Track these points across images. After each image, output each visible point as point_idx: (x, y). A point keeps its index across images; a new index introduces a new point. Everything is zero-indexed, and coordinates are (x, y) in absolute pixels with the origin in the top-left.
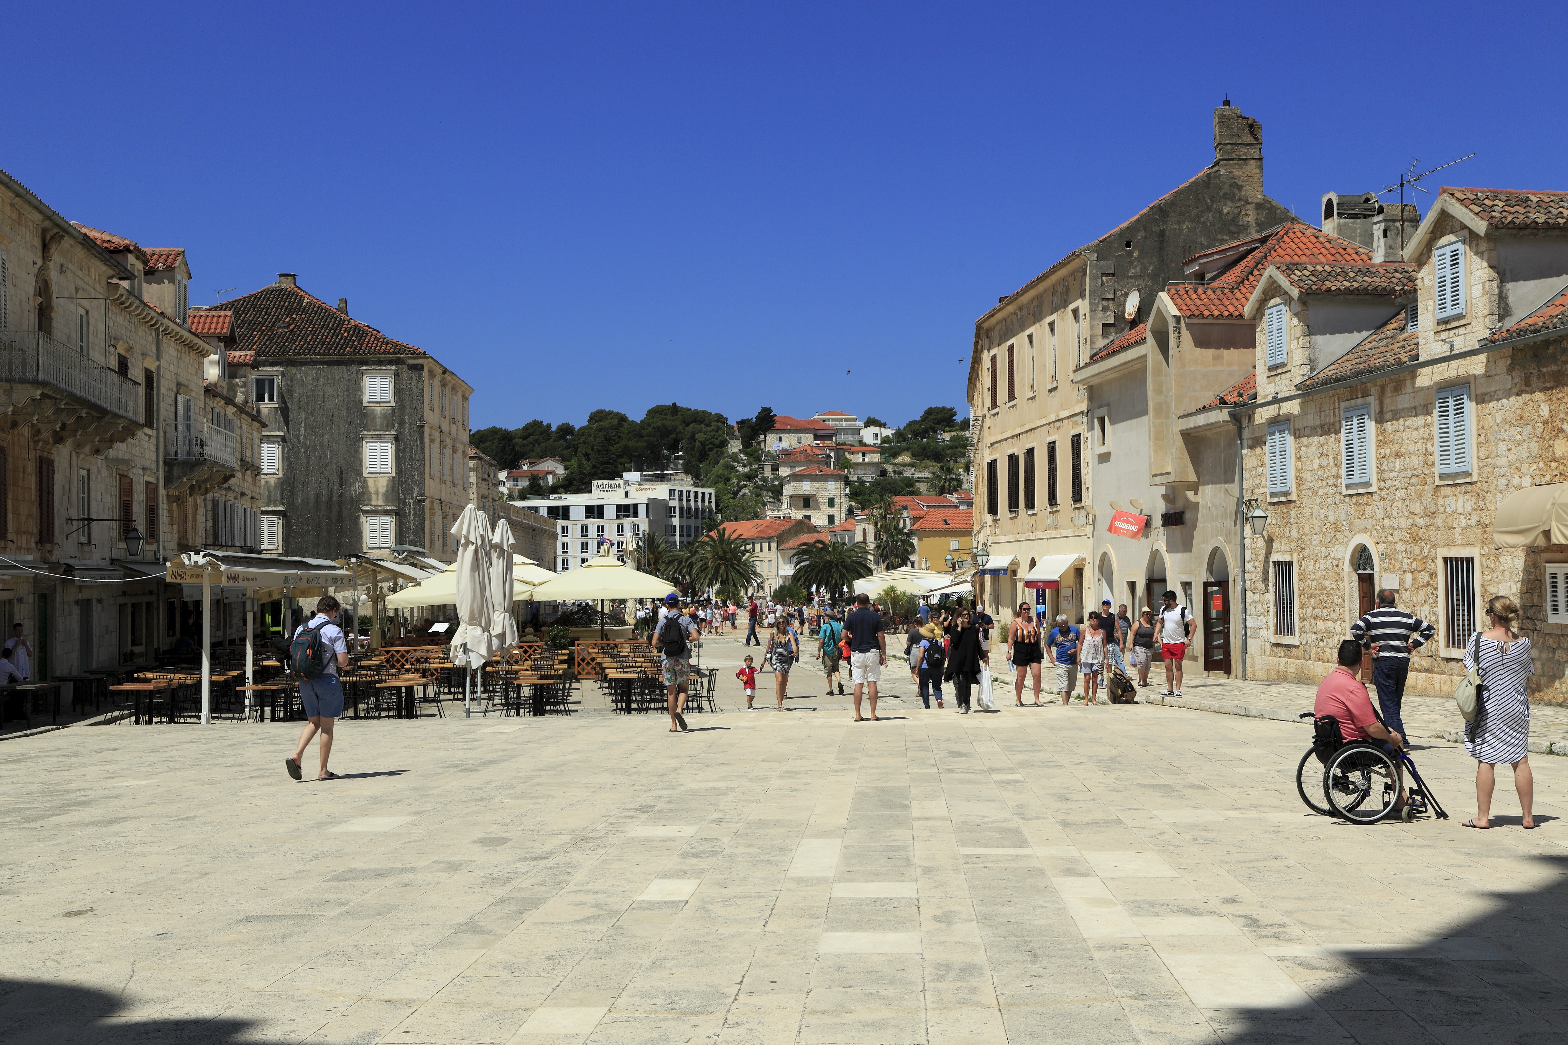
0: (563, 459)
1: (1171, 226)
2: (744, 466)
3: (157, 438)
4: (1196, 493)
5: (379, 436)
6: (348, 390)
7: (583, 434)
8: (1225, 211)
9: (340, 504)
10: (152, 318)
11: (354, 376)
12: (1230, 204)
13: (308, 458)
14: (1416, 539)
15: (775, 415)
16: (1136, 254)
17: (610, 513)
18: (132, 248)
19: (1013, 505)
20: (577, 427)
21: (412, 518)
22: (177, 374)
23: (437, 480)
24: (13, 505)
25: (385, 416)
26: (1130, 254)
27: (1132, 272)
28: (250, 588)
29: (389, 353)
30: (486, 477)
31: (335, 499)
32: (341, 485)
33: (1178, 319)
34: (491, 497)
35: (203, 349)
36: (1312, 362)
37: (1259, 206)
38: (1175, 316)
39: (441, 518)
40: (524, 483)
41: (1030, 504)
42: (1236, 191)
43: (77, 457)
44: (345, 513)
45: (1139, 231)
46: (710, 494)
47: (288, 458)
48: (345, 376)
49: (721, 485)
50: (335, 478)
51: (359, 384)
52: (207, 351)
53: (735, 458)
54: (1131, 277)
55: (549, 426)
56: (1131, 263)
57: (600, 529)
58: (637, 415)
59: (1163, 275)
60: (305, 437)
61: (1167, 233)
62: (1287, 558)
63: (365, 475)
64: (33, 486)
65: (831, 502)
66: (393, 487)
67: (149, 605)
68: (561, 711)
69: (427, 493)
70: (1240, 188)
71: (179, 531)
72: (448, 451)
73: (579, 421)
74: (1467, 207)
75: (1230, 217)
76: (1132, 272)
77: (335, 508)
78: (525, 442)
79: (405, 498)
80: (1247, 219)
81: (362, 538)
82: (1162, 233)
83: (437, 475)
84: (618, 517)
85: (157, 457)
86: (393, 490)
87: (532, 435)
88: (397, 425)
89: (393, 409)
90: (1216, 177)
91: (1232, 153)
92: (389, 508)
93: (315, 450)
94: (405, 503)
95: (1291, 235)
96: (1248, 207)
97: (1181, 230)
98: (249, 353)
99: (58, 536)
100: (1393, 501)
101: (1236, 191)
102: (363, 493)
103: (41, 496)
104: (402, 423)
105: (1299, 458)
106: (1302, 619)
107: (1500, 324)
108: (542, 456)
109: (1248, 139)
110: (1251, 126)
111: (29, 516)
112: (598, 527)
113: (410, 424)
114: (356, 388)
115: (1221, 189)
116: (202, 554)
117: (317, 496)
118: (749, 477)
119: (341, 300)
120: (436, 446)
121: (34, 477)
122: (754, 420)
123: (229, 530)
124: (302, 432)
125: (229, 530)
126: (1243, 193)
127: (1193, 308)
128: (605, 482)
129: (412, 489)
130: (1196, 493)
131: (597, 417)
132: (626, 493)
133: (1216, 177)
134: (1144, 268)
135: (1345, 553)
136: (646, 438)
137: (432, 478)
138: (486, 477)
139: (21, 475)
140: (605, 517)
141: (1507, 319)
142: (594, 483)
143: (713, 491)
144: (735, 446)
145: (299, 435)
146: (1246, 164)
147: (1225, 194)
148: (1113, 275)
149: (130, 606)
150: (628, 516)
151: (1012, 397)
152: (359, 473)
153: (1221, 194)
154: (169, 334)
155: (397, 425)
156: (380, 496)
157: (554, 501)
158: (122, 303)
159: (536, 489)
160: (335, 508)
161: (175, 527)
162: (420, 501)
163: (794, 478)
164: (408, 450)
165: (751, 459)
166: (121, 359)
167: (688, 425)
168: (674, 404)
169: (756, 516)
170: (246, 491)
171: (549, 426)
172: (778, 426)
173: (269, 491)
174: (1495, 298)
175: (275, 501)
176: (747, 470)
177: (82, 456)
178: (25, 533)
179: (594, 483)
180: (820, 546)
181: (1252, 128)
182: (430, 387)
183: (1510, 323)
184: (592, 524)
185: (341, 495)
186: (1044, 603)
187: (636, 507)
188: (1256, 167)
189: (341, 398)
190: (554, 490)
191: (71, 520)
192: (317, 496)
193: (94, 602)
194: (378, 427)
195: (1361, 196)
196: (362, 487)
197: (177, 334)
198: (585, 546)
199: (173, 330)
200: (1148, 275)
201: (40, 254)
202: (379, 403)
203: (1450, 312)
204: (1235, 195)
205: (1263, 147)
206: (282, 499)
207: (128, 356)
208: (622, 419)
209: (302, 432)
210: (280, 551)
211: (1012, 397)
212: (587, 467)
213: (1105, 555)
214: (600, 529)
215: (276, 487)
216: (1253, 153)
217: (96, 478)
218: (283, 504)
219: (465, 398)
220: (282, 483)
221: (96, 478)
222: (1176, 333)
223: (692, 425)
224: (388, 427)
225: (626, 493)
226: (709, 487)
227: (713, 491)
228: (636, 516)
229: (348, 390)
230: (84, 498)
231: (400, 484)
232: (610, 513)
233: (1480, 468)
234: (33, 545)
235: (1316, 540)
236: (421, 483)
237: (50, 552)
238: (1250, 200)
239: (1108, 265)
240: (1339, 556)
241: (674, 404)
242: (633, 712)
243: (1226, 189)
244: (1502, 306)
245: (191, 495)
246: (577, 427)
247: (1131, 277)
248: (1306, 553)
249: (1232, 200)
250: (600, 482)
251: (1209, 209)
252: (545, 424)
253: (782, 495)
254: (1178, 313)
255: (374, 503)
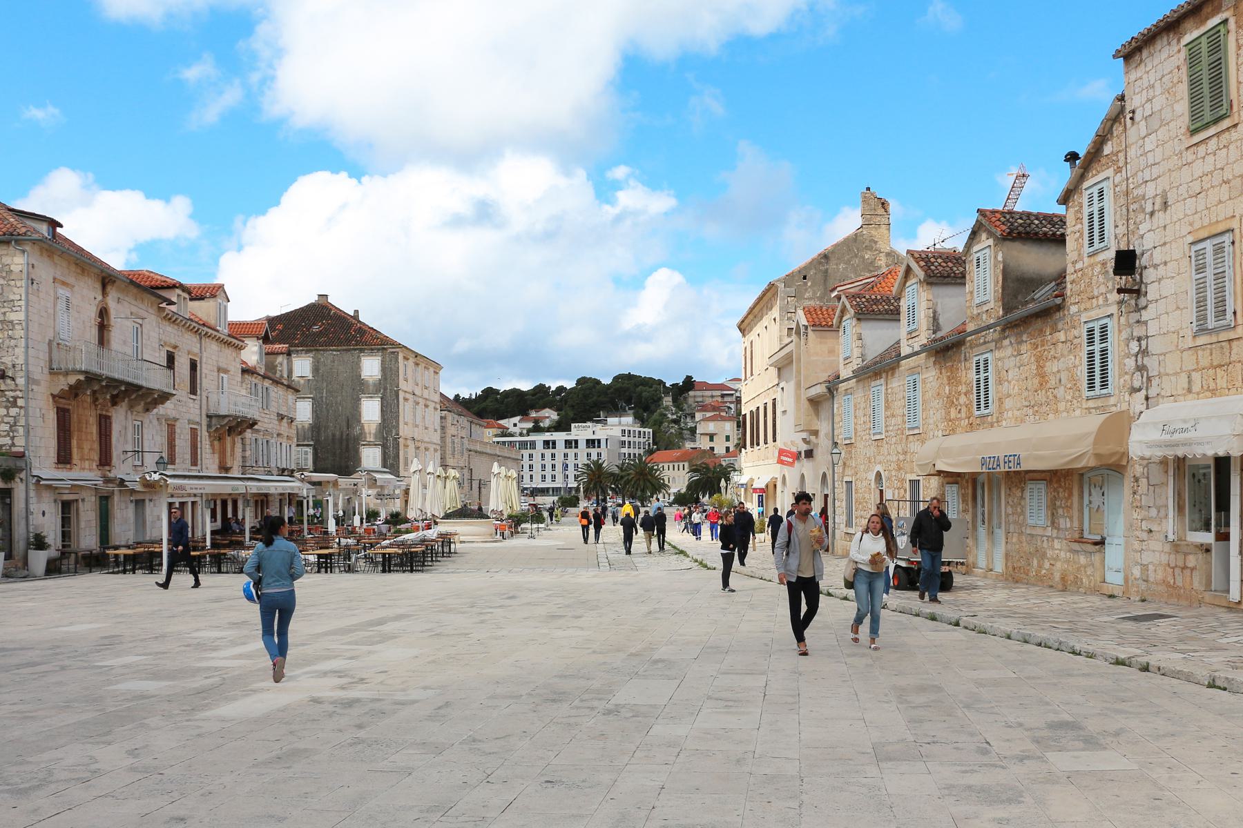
0: (558, 410)
1: (832, 266)
2: (673, 414)
3: (201, 400)
4: (817, 437)
5: (371, 397)
6: (352, 368)
7: (571, 393)
8: (867, 257)
9: (347, 440)
10: (194, 327)
11: (356, 360)
12: (869, 252)
13: (328, 411)
14: (900, 469)
15: (695, 381)
16: (809, 284)
17: (582, 445)
18: (177, 285)
19: (752, 444)
20: (568, 388)
21: (391, 449)
22: (217, 361)
23: (410, 425)
24: (78, 443)
25: (375, 385)
26: (806, 284)
27: (807, 295)
28: (272, 491)
29: (378, 345)
30: (455, 423)
31: (344, 437)
32: (348, 429)
33: (806, 327)
34: (460, 435)
35: (238, 345)
36: (863, 356)
37: (888, 255)
38: (804, 325)
39: (414, 449)
40: (530, 425)
41: (758, 444)
42: (874, 245)
43: (132, 414)
44: (350, 446)
45: (812, 269)
46: (649, 432)
47: (316, 411)
48: (351, 359)
49: (657, 427)
50: (344, 424)
51: (359, 364)
52: (242, 346)
53: (667, 408)
54: (806, 299)
55: (550, 387)
56: (806, 290)
57: (553, 456)
58: (606, 381)
59: (826, 298)
60: (326, 398)
61: (829, 271)
62: (907, 485)
63: (362, 422)
64: (95, 431)
65: (728, 438)
66: (380, 429)
67: (193, 503)
68: (420, 571)
69: (400, 434)
70: (876, 242)
71: (220, 458)
72: (420, 407)
73: (570, 384)
74: (918, 263)
75: (870, 261)
76: (807, 295)
77: (344, 443)
78: (534, 398)
79: (387, 437)
80: (880, 262)
81: (361, 462)
82: (826, 271)
83: (410, 422)
84: (566, 448)
85: (201, 412)
86: (380, 432)
87: (538, 393)
88: (382, 391)
89: (380, 380)
90: (860, 236)
91: (871, 220)
92: (377, 443)
93: (333, 406)
94: (387, 440)
95: (893, 274)
96: (881, 255)
97: (838, 269)
98: (284, 346)
99: (115, 461)
100: (891, 445)
101: (874, 245)
102: (361, 434)
103: (100, 437)
104: (385, 389)
105: (856, 417)
106: (856, 518)
107: (934, 336)
108: (544, 408)
109: (881, 211)
110: (883, 204)
111: (91, 449)
112: (552, 454)
113: (390, 390)
114: (357, 367)
115: (864, 243)
116: (158, 473)
117: (334, 435)
118: (676, 422)
119: (355, 311)
120: (409, 405)
121: (95, 426)
122: (681, 384)
123: (265, 457)
124: (324, 395)
125: (265, 457)
126: (878, 246)
127: (817, 320)
128: (580, 424)
129: (391, 431)
130: (817, 437)
131: (582, 381)
132: (594, 432)
133: (860, 236)
134: (814, 293)
135: (872, 476)
136: (610, 396)
137: (406, 424)
138: (455, 423)
139: (84, 426)
140: (579, 447)
141: (938, 332)
142: (573, 425)
143: (651, 430)
144: (667, 401)
145: (322, 397)
146: (880, 228)
147: (866, 246)
148: (795, 297)
149: (190, 504)
150: (571, 447)
151: (752, 375)
152: (359, 421)
153: (864, 246)
154: (210, 336)
155: (382, 391)
156: (372, 435)
157: (548, 436)
158: (170, 319)
159: (537, 429)
160: (344, 443)
161: (217, 456)
162: (396, 438)
163: (705, 419)
164: (389, 406)
165: (677, 410)
166: (169, 353)
167: (638, 387)
168: (629, 373)
169: (679, 448)
170: (282, 432)
171: (550, 387)
172: (696, 388)
173: (304, 432)
174: (931, 320)
175: (308, 438)
176: (675, 417)
177: (135, 413)
178: (87, 460)
179: (573, 425)
180: (705, 466)
181: (884, 204)
182: (405, 368)
183: (939, 335)
184: (548, 453)
185: (348, 434)
186: (762, 506)
187: (599, 441)
188: (886, 229)
189: (348, 374)
190: (548, 430)
191: (126, 452)
192: (334, 435)
193: (80, 500)
194: (371, 392)
195: (951, 249)
196: (361, 429)
197: (215, 336)
198: (544, 467)
199: (212, 334)
200: (817, 298)
201: (100, 292)
202: (371, 376)
203: (912, 327)
204: (872, 247)
205: (890, 217)
206: (313, 437)
207: (264, 346)
208: (598, 382)
209: (324, 395)
210: (311, 469)
211: (752, 375)
212: (571, 414)
213: (784, 475)
214: (553, 456)
215: (309, 428)
216: (884, 221)
217: (149, 425)
218: (312, 440)
219: (436, 373)
220: (312, 427)
221: (149, 425)
222: (805, 336)
223: (640, 387)
224: (377, 392)
225: (594, 432)
226: (650, 428)
227: (651, 430)
228: (599, 447)
229: (352, 368)
230: (138, 438)
231: (384, 428)
232: (582, 445)
233: (923, 425)
234: (95, 467)
235: (862, 467)
236: (397, 427)
237: (109, 471)
238: (882, 250)
239: (792, 290)
240: (870, 479)
241: (629, 373)
242: (414, 572)
243: (867, 243)
244: (935, 324)
245: (229, 435)
246: (568, 388)
247: (806, 299)
248: (858, 476)
249: (871, 250)
250: (577, 424)
251: (856, 256)
252: (547, 386)
253: (696, 432)
254: (806, 324)
255: (368, 440)
